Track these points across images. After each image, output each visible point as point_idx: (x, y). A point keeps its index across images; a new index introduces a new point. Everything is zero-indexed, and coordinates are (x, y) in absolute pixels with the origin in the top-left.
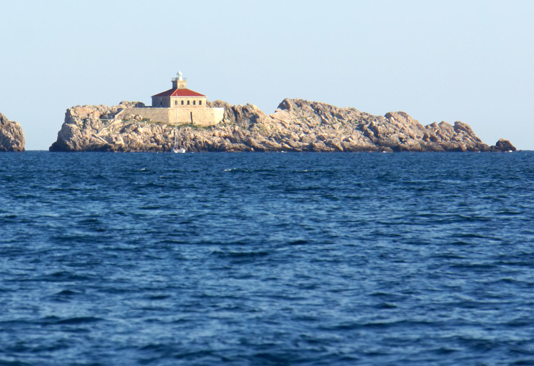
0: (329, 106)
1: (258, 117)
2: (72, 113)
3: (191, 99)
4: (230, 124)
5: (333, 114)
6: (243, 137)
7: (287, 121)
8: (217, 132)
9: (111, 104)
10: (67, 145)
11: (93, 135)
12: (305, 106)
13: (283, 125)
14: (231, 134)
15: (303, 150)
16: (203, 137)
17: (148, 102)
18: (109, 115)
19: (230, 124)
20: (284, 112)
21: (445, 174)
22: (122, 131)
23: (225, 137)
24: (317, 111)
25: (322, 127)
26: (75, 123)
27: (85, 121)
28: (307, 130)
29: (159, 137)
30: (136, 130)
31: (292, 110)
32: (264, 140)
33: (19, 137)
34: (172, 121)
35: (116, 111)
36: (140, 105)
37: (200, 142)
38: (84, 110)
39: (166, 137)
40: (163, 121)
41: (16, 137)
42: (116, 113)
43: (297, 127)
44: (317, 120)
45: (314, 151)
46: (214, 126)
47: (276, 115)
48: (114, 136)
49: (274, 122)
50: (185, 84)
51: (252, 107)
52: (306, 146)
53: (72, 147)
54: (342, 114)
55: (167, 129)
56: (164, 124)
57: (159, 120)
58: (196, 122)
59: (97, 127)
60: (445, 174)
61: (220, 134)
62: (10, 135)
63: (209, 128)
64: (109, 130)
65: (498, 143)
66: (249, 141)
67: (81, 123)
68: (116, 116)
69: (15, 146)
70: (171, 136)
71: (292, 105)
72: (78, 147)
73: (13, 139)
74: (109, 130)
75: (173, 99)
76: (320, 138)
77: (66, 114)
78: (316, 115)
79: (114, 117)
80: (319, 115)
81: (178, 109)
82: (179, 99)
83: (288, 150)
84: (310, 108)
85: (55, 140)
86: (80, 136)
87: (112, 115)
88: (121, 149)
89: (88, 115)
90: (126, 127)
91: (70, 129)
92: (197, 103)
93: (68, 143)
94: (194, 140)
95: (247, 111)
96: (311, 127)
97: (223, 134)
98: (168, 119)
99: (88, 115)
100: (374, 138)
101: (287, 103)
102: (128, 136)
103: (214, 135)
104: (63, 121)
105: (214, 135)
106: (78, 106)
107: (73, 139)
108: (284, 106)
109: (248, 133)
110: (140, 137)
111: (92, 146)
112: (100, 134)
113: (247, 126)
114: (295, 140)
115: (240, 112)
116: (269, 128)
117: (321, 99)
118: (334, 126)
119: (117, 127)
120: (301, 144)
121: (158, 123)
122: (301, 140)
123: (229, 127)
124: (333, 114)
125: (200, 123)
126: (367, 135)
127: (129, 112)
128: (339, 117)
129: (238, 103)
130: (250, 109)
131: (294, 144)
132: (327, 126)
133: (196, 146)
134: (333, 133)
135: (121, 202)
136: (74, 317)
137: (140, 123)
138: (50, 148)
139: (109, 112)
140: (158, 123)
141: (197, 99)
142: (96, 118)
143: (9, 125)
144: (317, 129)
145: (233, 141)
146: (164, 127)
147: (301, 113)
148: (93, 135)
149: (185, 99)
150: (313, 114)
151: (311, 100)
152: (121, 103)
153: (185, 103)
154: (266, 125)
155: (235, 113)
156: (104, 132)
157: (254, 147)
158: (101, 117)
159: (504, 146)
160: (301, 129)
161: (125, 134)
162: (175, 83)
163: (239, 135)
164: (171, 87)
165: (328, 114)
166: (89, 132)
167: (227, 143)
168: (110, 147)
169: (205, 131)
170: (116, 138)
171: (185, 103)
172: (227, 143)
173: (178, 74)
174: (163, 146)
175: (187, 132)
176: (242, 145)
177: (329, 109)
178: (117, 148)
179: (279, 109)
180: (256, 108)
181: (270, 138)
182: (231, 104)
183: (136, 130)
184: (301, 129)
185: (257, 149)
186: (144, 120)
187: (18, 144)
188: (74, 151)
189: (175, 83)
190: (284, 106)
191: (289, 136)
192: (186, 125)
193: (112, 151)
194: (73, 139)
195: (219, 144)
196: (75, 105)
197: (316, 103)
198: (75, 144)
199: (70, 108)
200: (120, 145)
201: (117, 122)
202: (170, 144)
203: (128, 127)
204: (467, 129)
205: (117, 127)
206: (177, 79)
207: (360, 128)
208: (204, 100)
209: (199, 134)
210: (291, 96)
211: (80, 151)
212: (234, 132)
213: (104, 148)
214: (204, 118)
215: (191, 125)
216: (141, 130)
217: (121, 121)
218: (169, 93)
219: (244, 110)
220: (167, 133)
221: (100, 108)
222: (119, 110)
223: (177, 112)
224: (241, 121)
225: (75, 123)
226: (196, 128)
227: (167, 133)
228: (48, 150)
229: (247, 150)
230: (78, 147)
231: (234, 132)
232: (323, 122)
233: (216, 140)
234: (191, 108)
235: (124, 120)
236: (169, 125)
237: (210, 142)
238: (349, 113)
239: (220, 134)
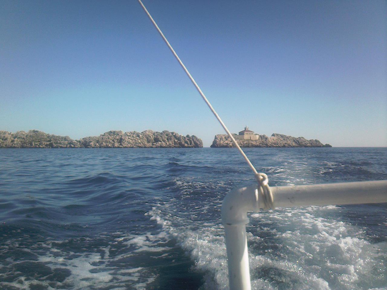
2: (217, 136)
6: (265, 143)
7: (275, 139)
12: (279, 135)
17: (238, 134)
20: (273, 137)
21: (144, 254)
23: (260, 143)
29: (242, 143)
33: (201, 143)
39: (243, 143)
41: (200, 143)
58: (252, 139)
60: (144, 254)
62: (198, 143)
63: (256, 141)
65: (326, 145)
66: (267, 144)
67: (219, 139)
72: (219, 146)
73: (199, 143)
75: (245, 133)
85: (212, 144)
91: (216, 141)
98: (244, 138)
100: (298, 144)
104: (214, 139)
105: (257, 143)
114: (279, 144)
126: (296, 143)
130: (265, 136)
131: (279, 145)
133: (252, 145)
135: (183, 217)
136: (149, 250)
153: (249, 134)
155: (261, 137)
159: (328, 146)
164: (244, 130)
169: (255, 142)
171: (249, 134)
172: (261, 145)
189: (245, 128)
192: (249, 140)
204: (318, 141)
206: (246, 127)
207: (294, 141)
212: (262, 142)
215: (250, 140)
219: (263, 136)
226: (252, 141)
230: (219, 146)
232: (284, 139)
233: (258, 144)
236: (244, 140)
237: (256, 145)
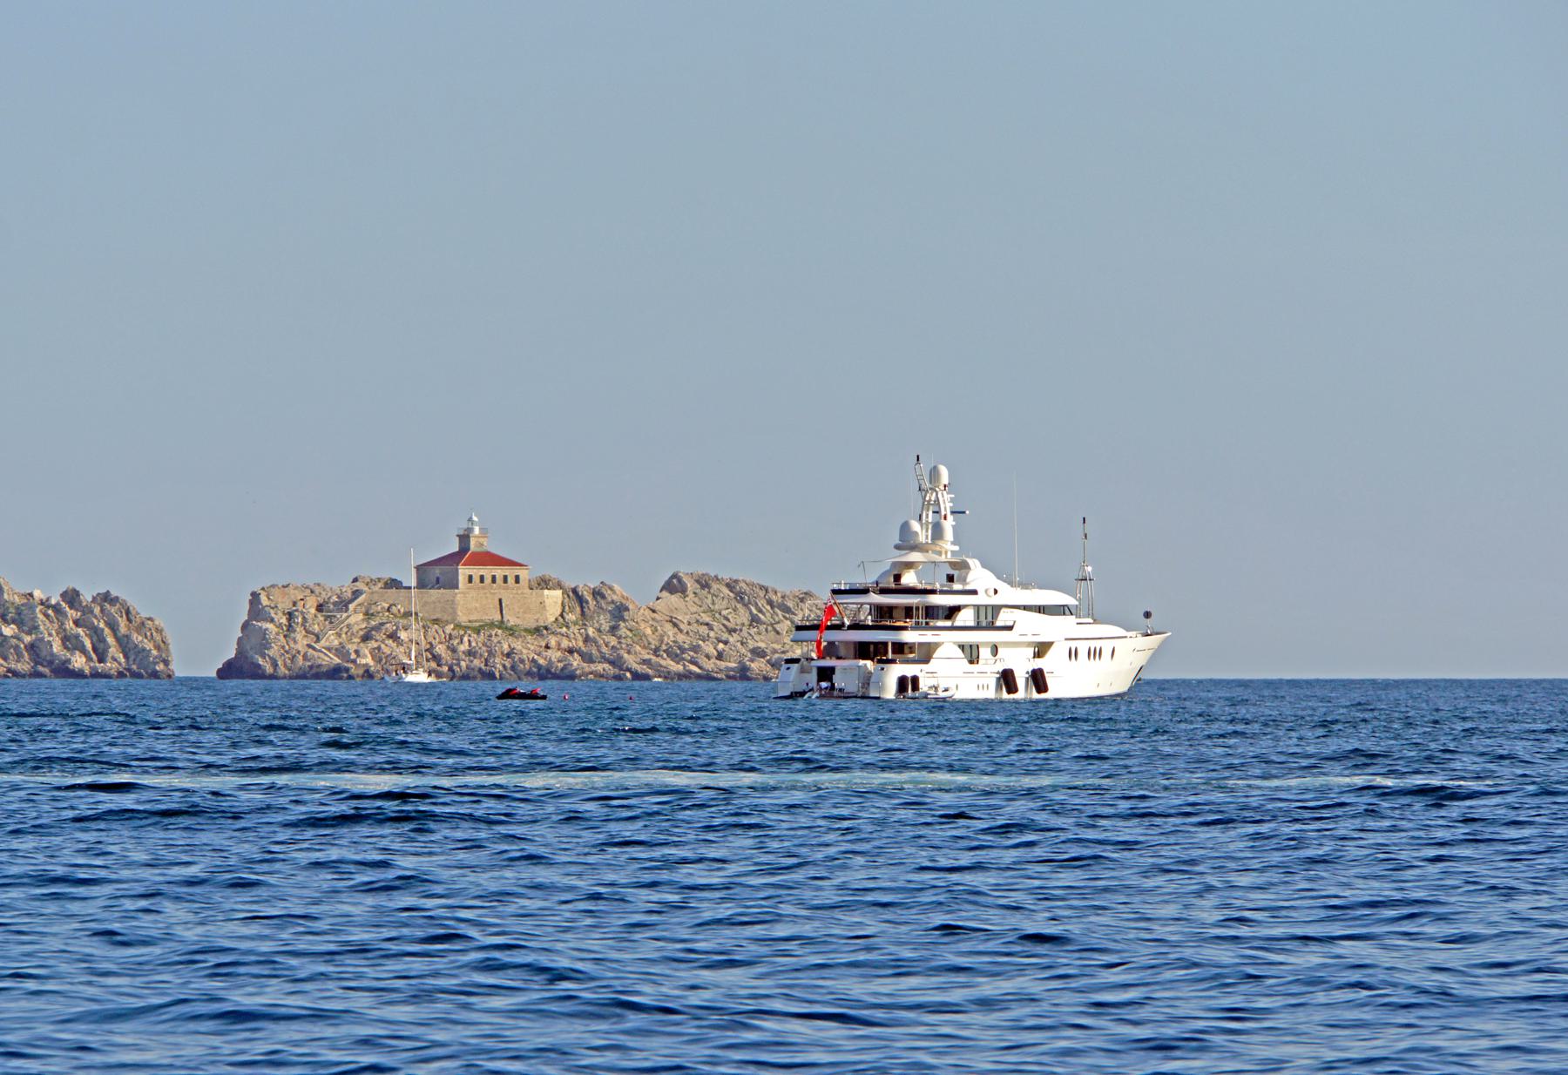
0: (761, 587)
1: (627, 609)
2: (264, 600)
3: (499, 572)
4: (575, 623)
5: (770, 603)
6: (604, 649)
8: (553, 641)
9: (337, 583)
10: (259, 666)
11: (309, 646)
12: (715, 586)
13: (675, 625)
14: (581, 644)
15: (729, 677)
16: (527, 649)
18: (335, 604)
19: (575, 623)
20: (675, 599)
22: (366, 638)
23: (571, 651)
24: (740, 596)
25: (753, 631)
26: (272, 620)
27: (290, 616)
28: (725, 636)
30: (393, 636)
31: (691, 595)
32: (647, 657)
34: (463, 618)
35: (349, 595)
36: (393, 584)
37: (522, 661)
38: (284, 594)
40: (446, 617)
42: (351, 601)
43: (703, 630)
44: (742, 617)
45: (749, 679)
46: (546, 628)
47: (659, 606)
48: (351, 648)
49: (657, 624)
50: (484, 541)
51: (611, 588)
52: (732, 669)
53: (269, 669)
54: (790, 604)
55: (455, 633)
56: (447, 623)
57: (437, 616)
58: (511, 620)
59: (316, 628)
61: (559, 644)
62: (149, 646)
64: (339, 635)
67: (284, 620)
68: (351, 607)
69: (160, 667)
70: (464, 647)
71: (691, 585)
72: (282, 670)
74: (339, 635)
75: (463, 572)
76: (758, 653)
77: (251, 602)
78: (739, 606)
79: (346, 606)
80: (745, 605)
81: (473, 593)
82: (476, 571)
83: (699, 677)
84: (726, 591)
86: (1146, 676)
87: (343, 605)
88: (368, 674)
89: (294, 604)
90: (373, 629)
92: (511, 580)
93: (261, 661)
94: (508, 655)
95: (603, 597)
96: (731, 631)
97: (565, 643)
99: (294, 604)
101: (680, 580)
102: (379, 648)
103: (547, 647)
105: (547, 647)
106: (273, 586)
107: (271, 652)
108: (674, 586)
109: (613, 641)
110: (402, 649)
111: (311, 667)
112: (323, 643)
113: (605, 627)
114: (708, 657)
115: (589, 598)
116: (649, 631)
117: (746, 575)
118: (778, 627)
119: (356, 628)
120: (722, 665)
121: (436, 621)
122: (720, 656)
123: (575, 629)
124: (770, 603)
125: (519, 622)
127: (376, 597)
128: (787, 610)
129: (586, 582)
130: (608, 593)
131: (709, 665)
132: (762, 628)
134: (776, 642)
137: (403, 622)
138: (219, 671)
139: (335, 598)
140: (436, 621)
141: (510, 572)
142: (313, 611)
143: (143, 624)
144: (744, 633)
145: (588, 658)
146: (449, 628)
147: (709, 601)
148: (309, 646)
149: (487, 571)
150: (734, 603)
151: (726, 575)
152: (355, 580)
153: (488, 580)
154: (643, 625)
156: (331, 639)
157: (629, 670)
158: (320, 608)
160: (712, 634)
161: (373, 644)
162: (464, 538)
163: (598, 647)
165: (762, 603)
166: (301, 641)
167: (576, 661)
168: (347, 670)
170: (357, 652)
171: (488, 580)
172: (576, 661)
173: (470, 519)
174: (451, 669)
175: (495, 640)
176: (606, 666)
177: (762, 594)
178: (361, 672)
179: (665, 594)
180: (619, 591)
181: (656, 652)
182: (569, 584)
183: (393, 636)
184: (712, 634)
185: (637, 676)
186: (407, 614)
187: (166, 663)
188: (272, 677)
189: (464, 538)
190: (674, 586)
191: (696, 649)
192: (492, 625)
193: (351, 677)
194: (271, 652)
195: (560, 665)
196: (266, 585)
197: (736, 581)
198: (275, 665)
199: (257, 589)
200: (366, 665)
201: (356, 619)
202: (463, 664)
203: (377, 628)
205: (356, 628)
208: (524, 574)
209: (518, 645)
210: (687, 569)
211: (284, 677)
212: (587, 639)
213: (335, 673)
214: (527, 614)
215: (501, 625)
216: (403, 635)
217: (361, 616)
218: (454, 559)
219: (597, 594)
220: (455, 642)
221: (317, 590)
222: (356, 594)
223: (471, 599)
224: (592, 618)
225: (272, 620)
226: (512, 631)
227: (455, 642)
228: (214, 674)
229: (618, 678)
231: (587, 639)
232: (754, 620)
233: (554, 655)
234: (499, 591)
235: (368, 615)
236: (458, 626)
238: (802, 600)
239: (559, 644)
